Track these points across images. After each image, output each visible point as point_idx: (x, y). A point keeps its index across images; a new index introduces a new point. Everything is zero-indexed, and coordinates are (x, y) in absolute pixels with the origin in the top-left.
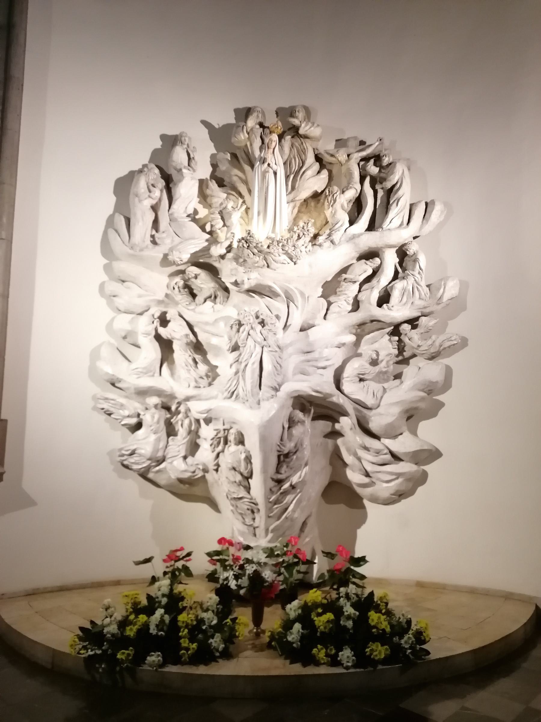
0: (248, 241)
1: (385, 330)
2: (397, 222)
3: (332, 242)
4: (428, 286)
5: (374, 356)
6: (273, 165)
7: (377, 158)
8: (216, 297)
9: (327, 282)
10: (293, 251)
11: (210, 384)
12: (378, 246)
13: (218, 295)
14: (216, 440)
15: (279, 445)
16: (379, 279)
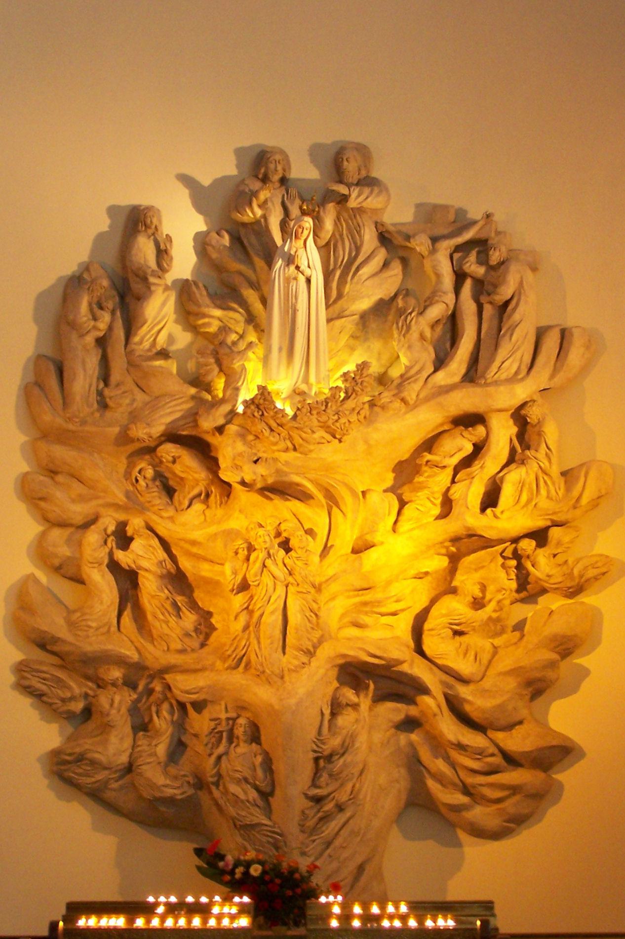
0: (261, 407)
2: (511, 367)
3: (403, 400)
4: (564, 474)
5: (478, 594)
6: (304, 266)
7: (481, 245)
8: (208, 496)
9: (400, 463)
10: (337, 421)
11: (203, 645)
13: (212, 492)
14: (214, 737)
16: (482, 462)
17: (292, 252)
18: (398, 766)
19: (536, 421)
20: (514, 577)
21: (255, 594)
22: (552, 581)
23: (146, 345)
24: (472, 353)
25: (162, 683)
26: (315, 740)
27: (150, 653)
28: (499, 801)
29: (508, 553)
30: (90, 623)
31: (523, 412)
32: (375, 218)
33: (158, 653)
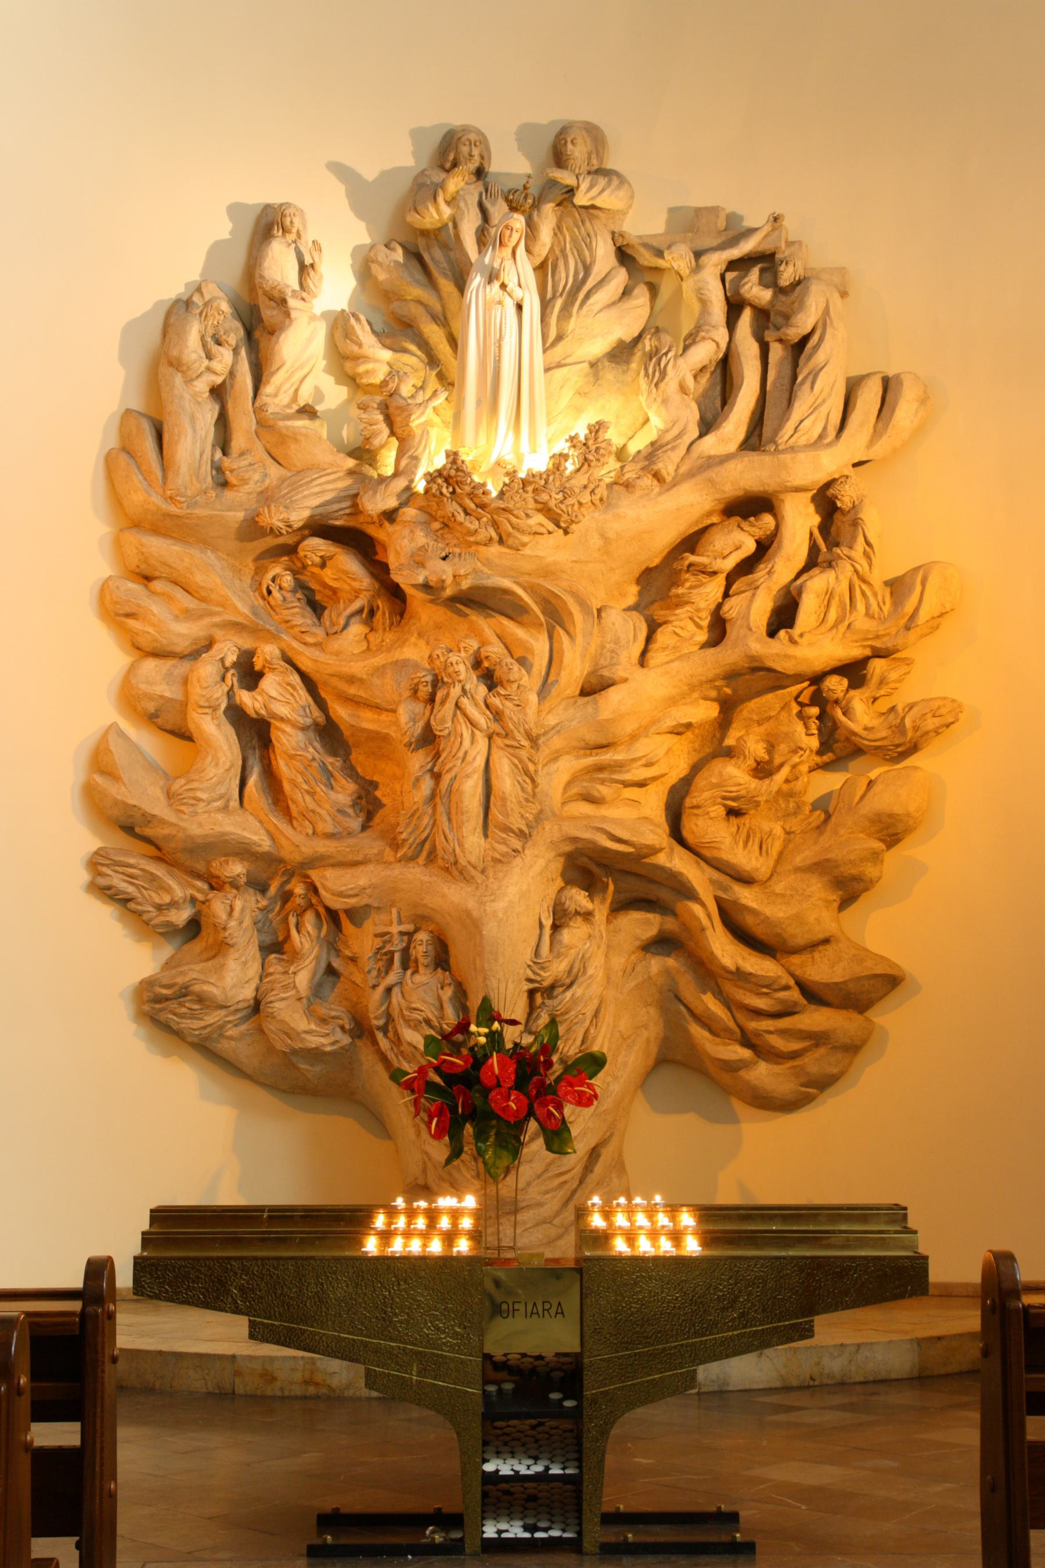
0: (451, 481)
1: (788, 690)
2: (812, 428)
3: (657, 476)
6: (512, 285)
8: (372, 613)
9: (648, 571)
10: (561, 502)
12: (767, 488)
13: (378, 607)
15: (529, 966)
16: (770, 566)
17: (496, 265)
18: (647, 1005)
19: (850, 505)
20: (816, 732)
21: (444, 750)
22: (871, 737)
23: (284, 398)
24: (753, 413)
25: (306, 883)
26: (531, 964)
27: (287, 838)
28: (794, 1055)
29: (805, 698)
30: (199, 794)
31: (831, 492)
32: (612, 227)
33: (298, 838)
